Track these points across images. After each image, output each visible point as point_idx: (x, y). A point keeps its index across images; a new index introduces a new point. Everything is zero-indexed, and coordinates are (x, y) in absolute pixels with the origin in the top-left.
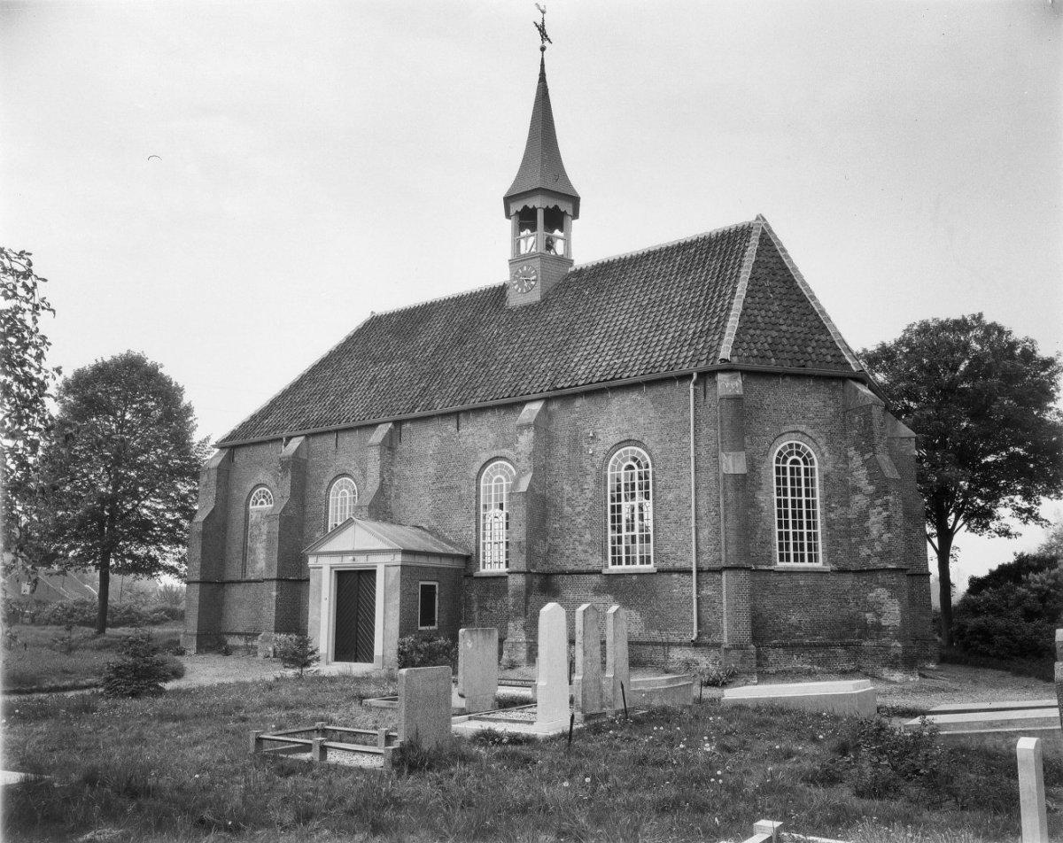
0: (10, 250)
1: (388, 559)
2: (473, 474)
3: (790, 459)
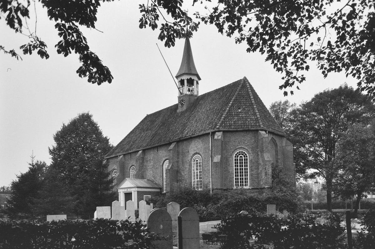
0: (289, 50)
1: (134, 189)
2: (161, 164)
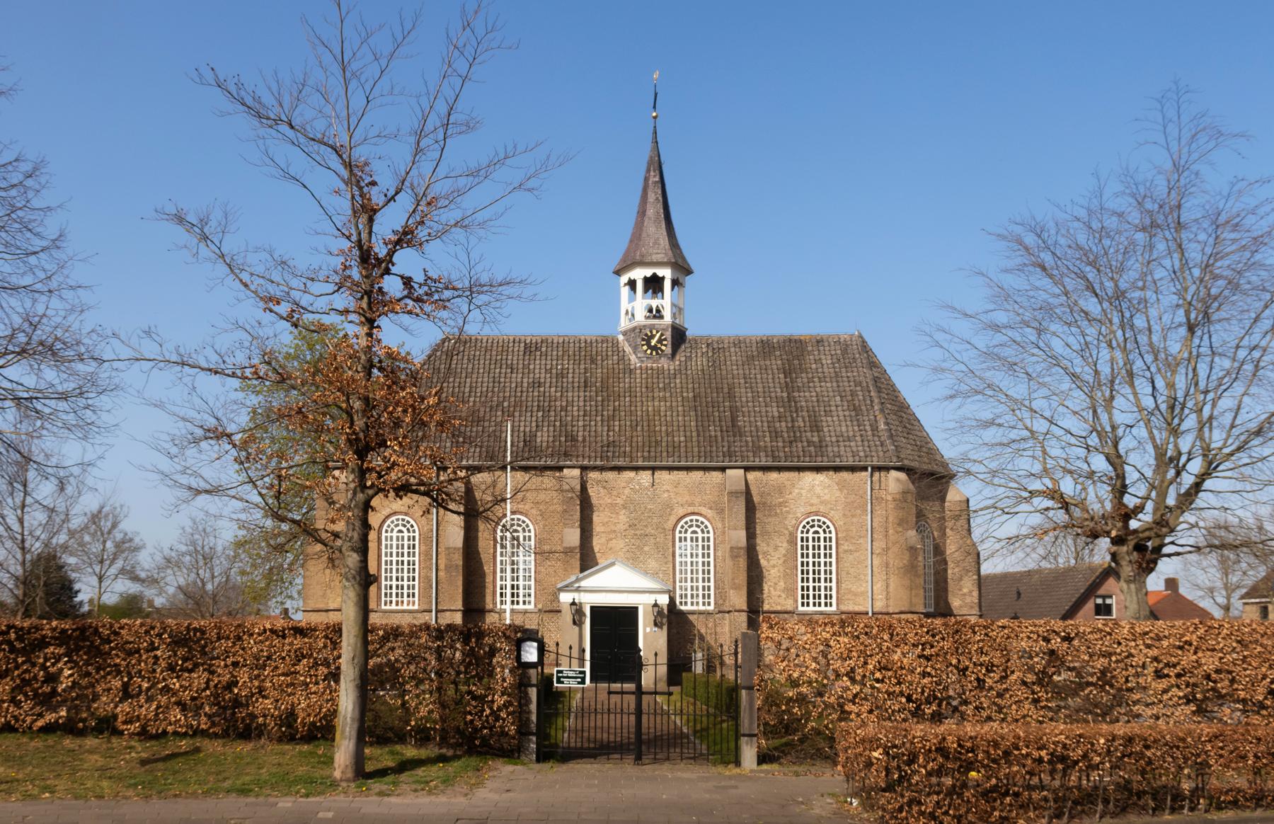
3: (396, 529)
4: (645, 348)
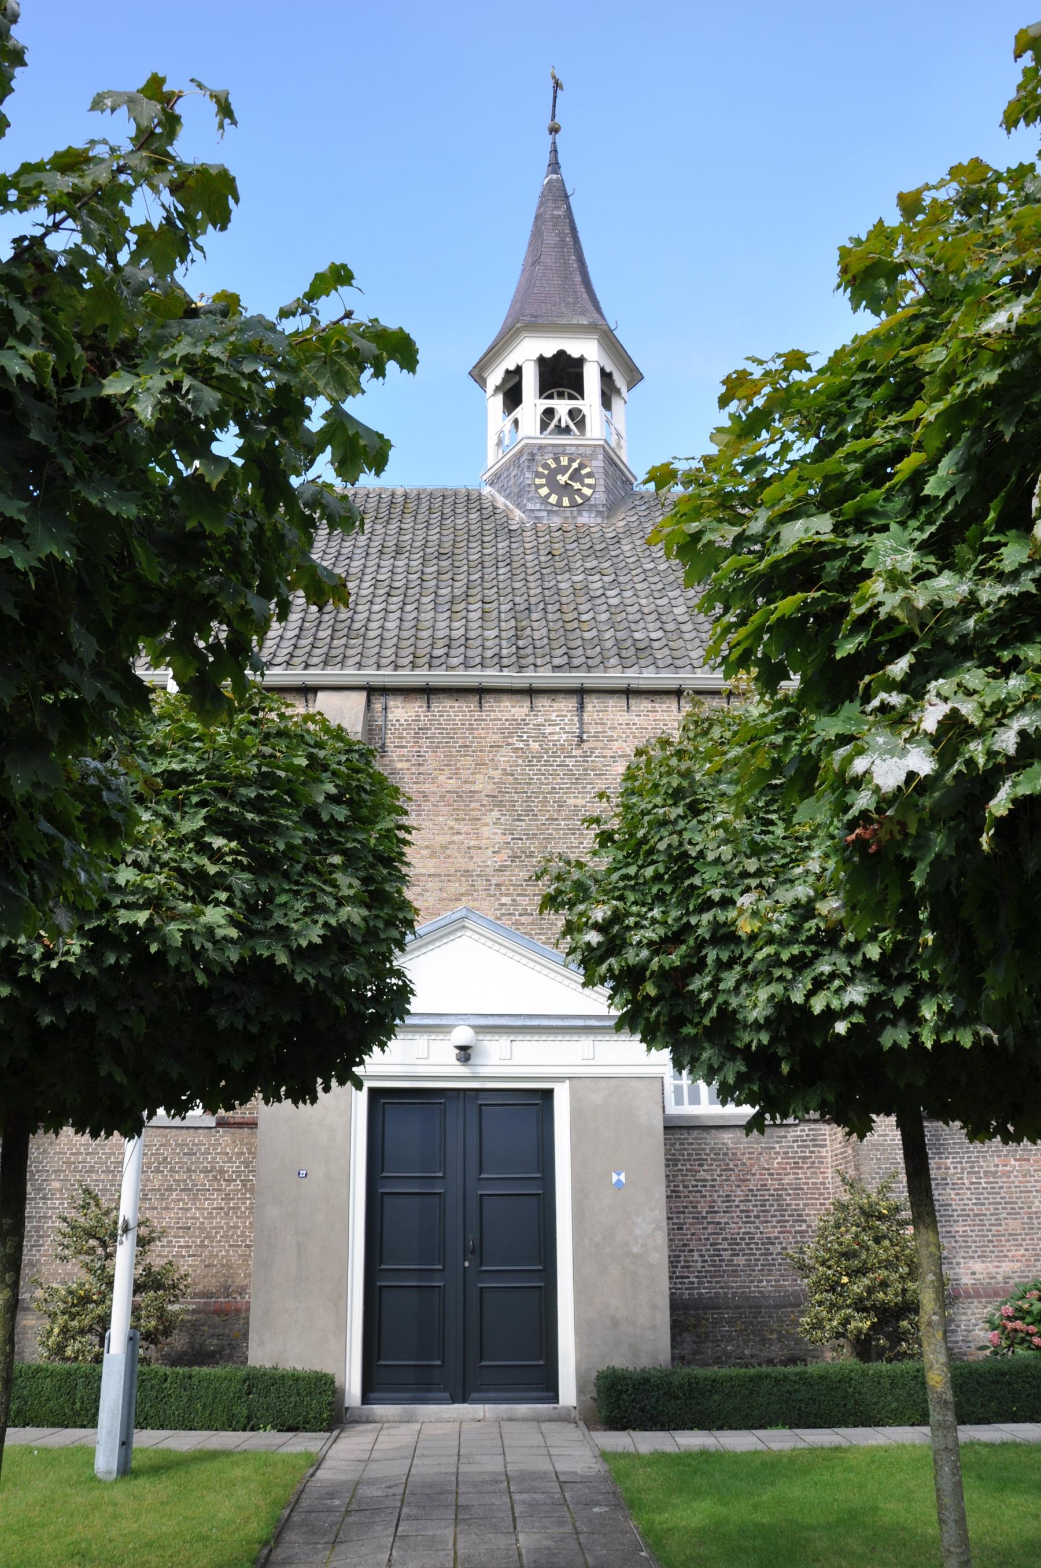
4: (544, 491)
